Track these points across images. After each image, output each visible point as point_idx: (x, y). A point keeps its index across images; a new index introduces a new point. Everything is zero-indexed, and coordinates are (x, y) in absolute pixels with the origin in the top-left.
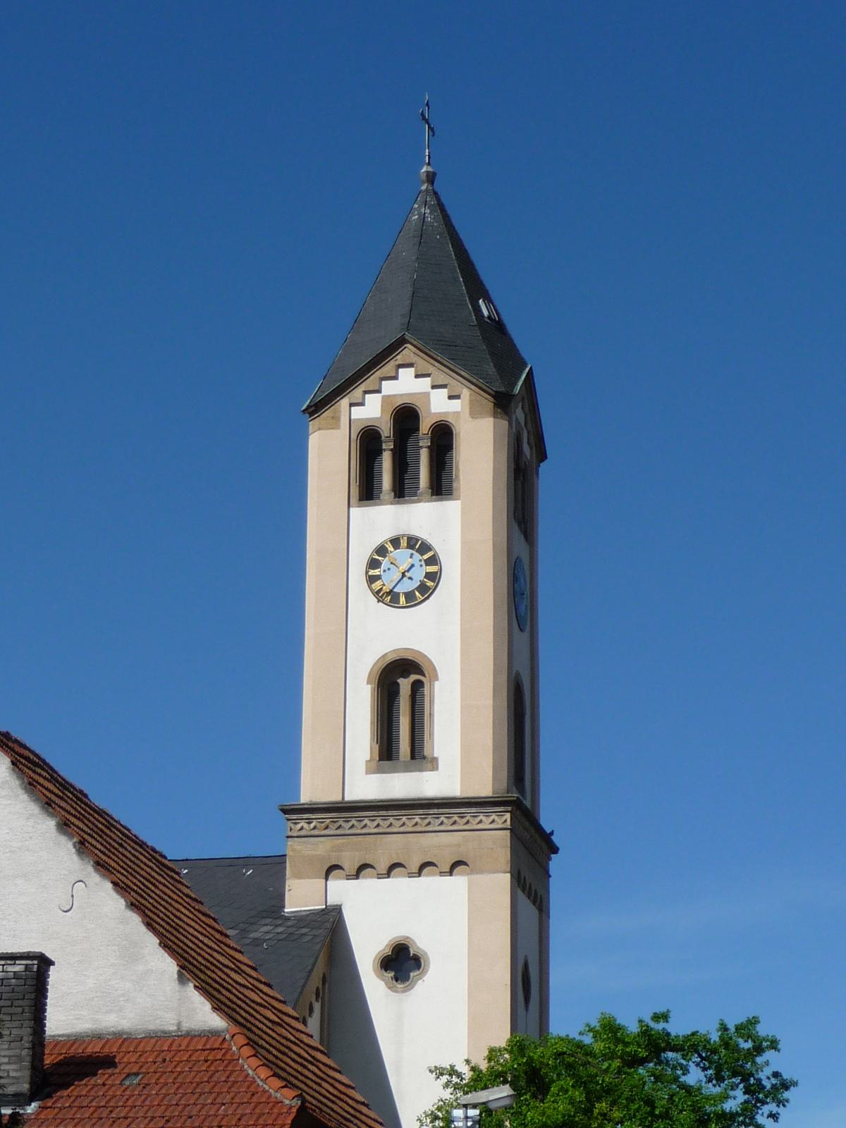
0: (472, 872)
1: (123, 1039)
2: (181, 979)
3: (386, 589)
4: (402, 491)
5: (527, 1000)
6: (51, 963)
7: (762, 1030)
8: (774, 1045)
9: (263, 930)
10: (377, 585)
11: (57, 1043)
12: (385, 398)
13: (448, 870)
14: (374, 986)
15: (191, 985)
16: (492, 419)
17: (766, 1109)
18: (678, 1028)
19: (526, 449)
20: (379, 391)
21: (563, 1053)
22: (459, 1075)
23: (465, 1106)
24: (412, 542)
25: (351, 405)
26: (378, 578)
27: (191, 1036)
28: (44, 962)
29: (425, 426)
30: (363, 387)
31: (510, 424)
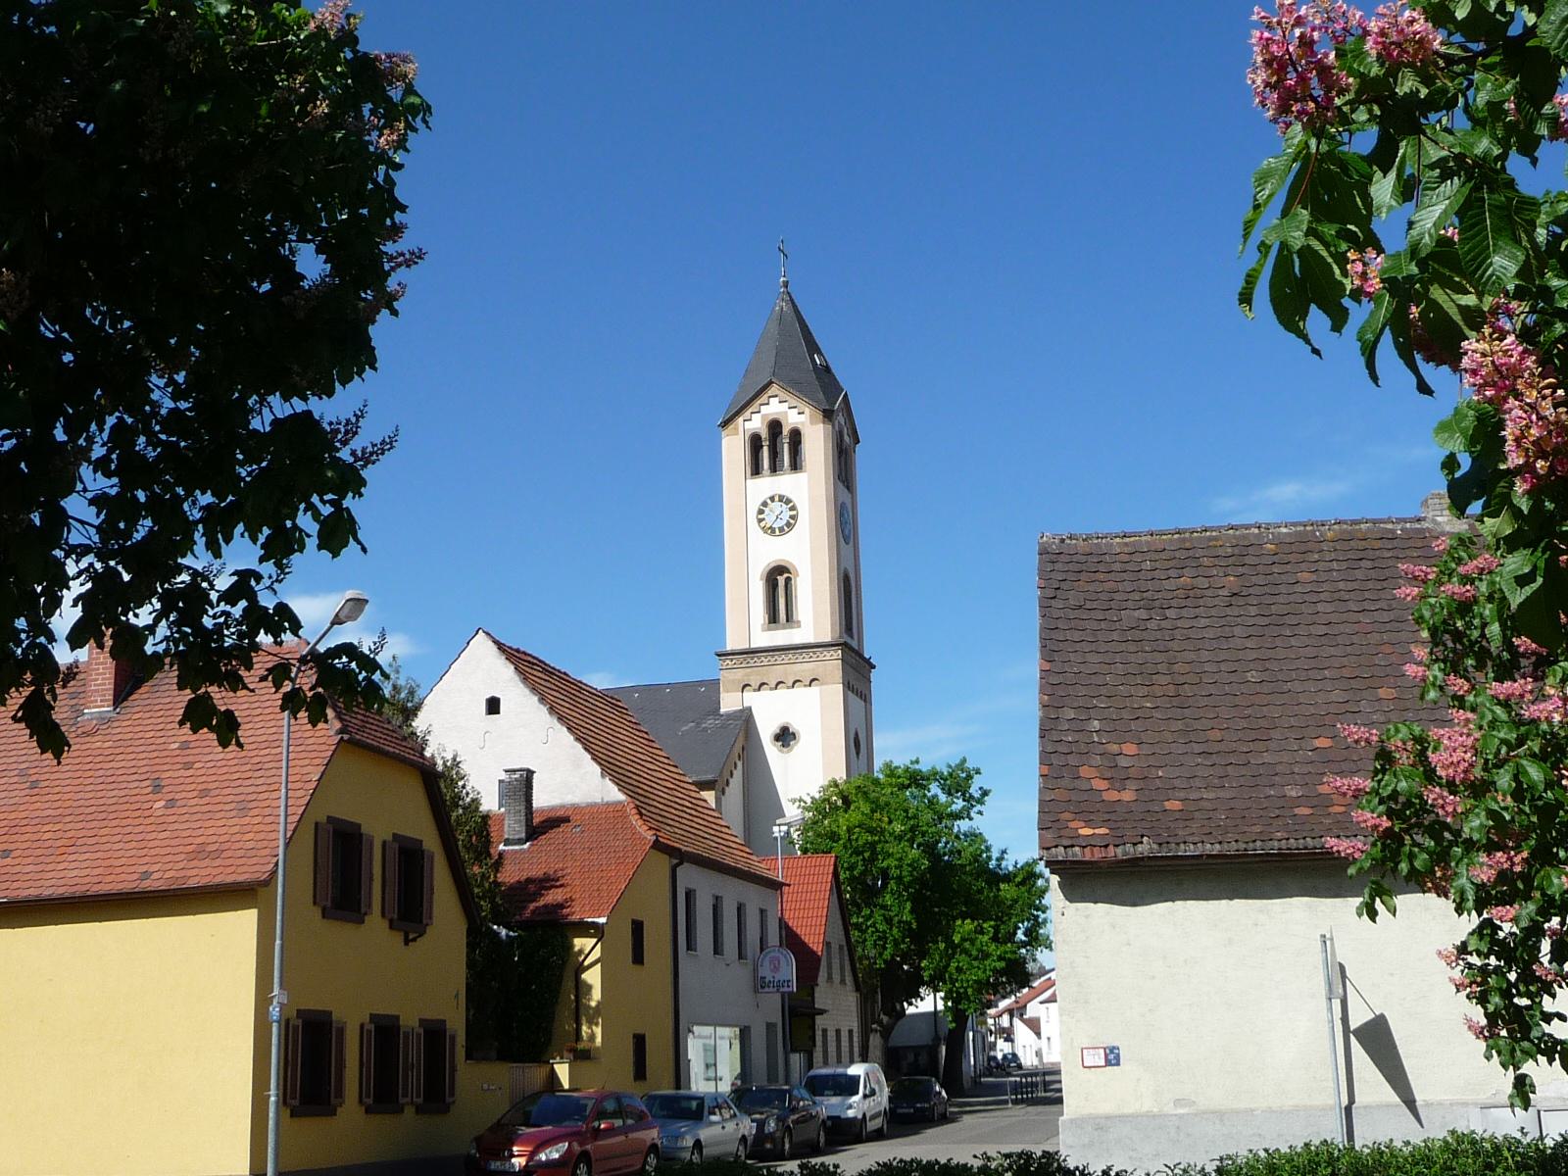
0: (822, 684)
1: (576, 808)
2: (603, 776)
3: (768, 526)
4: (774, 469)
5: (858, 753)
6: (533, 772)
7: (969, 765)
8: (978, 772)
9: (709, 723)
10: (763, 524)
11: (542, 811)
13: (808, 683)
14: (771, 750)
15: (607, 778)
16: (822, 425)
17: (975, 809)
18: (924, 767)
19: (846, 438)
20: (759, 412)
21: (859, 787)
22: (805, 803)
23: (779, 825)
24: (781, 498)
25: (745, 421)
26: (764, 519)
27: (608, 804)
28: (530, 773)
29: (786, 431)
30: (750, 410)
31: (833, 426)
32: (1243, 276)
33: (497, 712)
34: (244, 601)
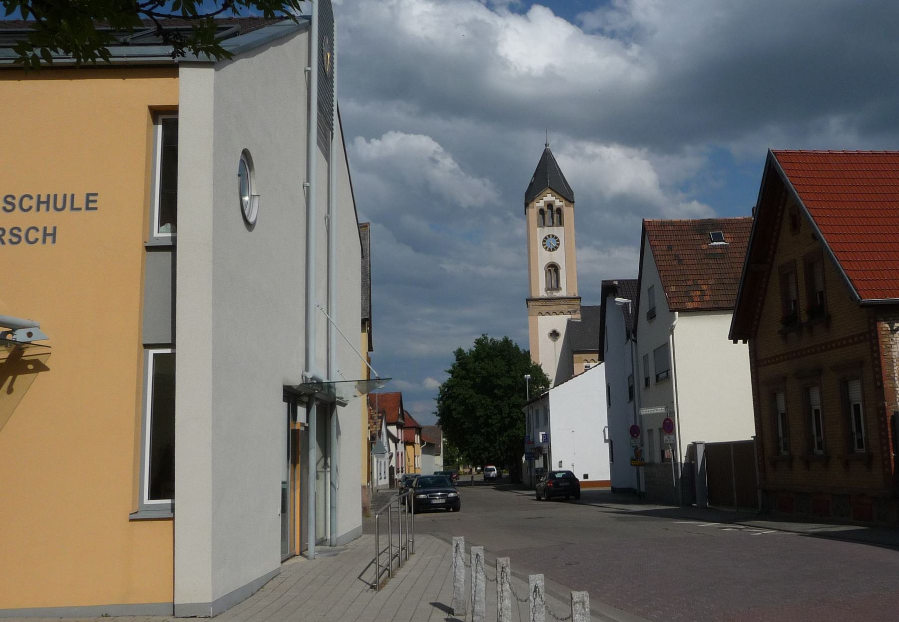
12: (545, 202)
20: (543, 199)
32: (543, 237)
33: (54, 227)
34: (557, 477)
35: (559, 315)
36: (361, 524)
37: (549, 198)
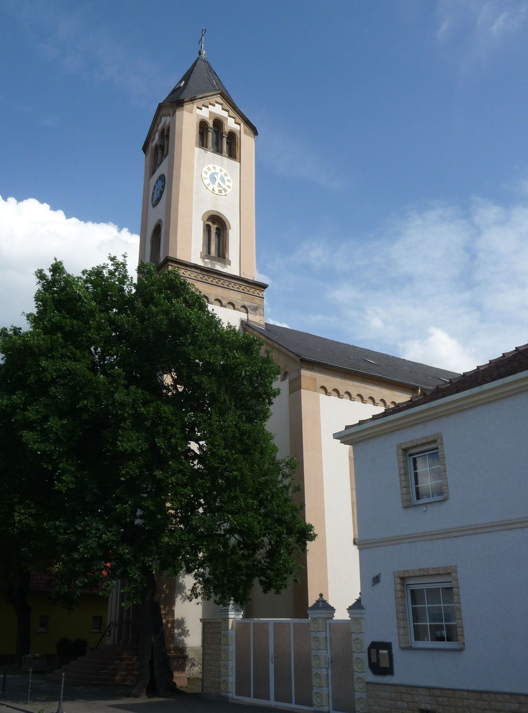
12: (210, 113)
35: (225, 307)
36: (178, 258)
37: (218, 110)
